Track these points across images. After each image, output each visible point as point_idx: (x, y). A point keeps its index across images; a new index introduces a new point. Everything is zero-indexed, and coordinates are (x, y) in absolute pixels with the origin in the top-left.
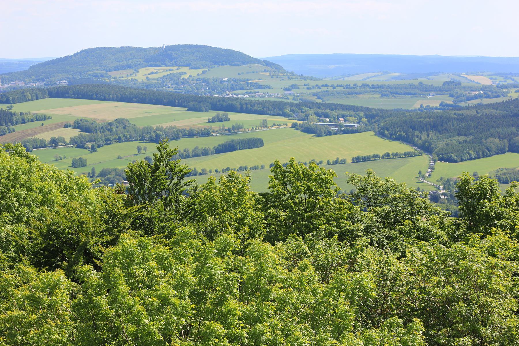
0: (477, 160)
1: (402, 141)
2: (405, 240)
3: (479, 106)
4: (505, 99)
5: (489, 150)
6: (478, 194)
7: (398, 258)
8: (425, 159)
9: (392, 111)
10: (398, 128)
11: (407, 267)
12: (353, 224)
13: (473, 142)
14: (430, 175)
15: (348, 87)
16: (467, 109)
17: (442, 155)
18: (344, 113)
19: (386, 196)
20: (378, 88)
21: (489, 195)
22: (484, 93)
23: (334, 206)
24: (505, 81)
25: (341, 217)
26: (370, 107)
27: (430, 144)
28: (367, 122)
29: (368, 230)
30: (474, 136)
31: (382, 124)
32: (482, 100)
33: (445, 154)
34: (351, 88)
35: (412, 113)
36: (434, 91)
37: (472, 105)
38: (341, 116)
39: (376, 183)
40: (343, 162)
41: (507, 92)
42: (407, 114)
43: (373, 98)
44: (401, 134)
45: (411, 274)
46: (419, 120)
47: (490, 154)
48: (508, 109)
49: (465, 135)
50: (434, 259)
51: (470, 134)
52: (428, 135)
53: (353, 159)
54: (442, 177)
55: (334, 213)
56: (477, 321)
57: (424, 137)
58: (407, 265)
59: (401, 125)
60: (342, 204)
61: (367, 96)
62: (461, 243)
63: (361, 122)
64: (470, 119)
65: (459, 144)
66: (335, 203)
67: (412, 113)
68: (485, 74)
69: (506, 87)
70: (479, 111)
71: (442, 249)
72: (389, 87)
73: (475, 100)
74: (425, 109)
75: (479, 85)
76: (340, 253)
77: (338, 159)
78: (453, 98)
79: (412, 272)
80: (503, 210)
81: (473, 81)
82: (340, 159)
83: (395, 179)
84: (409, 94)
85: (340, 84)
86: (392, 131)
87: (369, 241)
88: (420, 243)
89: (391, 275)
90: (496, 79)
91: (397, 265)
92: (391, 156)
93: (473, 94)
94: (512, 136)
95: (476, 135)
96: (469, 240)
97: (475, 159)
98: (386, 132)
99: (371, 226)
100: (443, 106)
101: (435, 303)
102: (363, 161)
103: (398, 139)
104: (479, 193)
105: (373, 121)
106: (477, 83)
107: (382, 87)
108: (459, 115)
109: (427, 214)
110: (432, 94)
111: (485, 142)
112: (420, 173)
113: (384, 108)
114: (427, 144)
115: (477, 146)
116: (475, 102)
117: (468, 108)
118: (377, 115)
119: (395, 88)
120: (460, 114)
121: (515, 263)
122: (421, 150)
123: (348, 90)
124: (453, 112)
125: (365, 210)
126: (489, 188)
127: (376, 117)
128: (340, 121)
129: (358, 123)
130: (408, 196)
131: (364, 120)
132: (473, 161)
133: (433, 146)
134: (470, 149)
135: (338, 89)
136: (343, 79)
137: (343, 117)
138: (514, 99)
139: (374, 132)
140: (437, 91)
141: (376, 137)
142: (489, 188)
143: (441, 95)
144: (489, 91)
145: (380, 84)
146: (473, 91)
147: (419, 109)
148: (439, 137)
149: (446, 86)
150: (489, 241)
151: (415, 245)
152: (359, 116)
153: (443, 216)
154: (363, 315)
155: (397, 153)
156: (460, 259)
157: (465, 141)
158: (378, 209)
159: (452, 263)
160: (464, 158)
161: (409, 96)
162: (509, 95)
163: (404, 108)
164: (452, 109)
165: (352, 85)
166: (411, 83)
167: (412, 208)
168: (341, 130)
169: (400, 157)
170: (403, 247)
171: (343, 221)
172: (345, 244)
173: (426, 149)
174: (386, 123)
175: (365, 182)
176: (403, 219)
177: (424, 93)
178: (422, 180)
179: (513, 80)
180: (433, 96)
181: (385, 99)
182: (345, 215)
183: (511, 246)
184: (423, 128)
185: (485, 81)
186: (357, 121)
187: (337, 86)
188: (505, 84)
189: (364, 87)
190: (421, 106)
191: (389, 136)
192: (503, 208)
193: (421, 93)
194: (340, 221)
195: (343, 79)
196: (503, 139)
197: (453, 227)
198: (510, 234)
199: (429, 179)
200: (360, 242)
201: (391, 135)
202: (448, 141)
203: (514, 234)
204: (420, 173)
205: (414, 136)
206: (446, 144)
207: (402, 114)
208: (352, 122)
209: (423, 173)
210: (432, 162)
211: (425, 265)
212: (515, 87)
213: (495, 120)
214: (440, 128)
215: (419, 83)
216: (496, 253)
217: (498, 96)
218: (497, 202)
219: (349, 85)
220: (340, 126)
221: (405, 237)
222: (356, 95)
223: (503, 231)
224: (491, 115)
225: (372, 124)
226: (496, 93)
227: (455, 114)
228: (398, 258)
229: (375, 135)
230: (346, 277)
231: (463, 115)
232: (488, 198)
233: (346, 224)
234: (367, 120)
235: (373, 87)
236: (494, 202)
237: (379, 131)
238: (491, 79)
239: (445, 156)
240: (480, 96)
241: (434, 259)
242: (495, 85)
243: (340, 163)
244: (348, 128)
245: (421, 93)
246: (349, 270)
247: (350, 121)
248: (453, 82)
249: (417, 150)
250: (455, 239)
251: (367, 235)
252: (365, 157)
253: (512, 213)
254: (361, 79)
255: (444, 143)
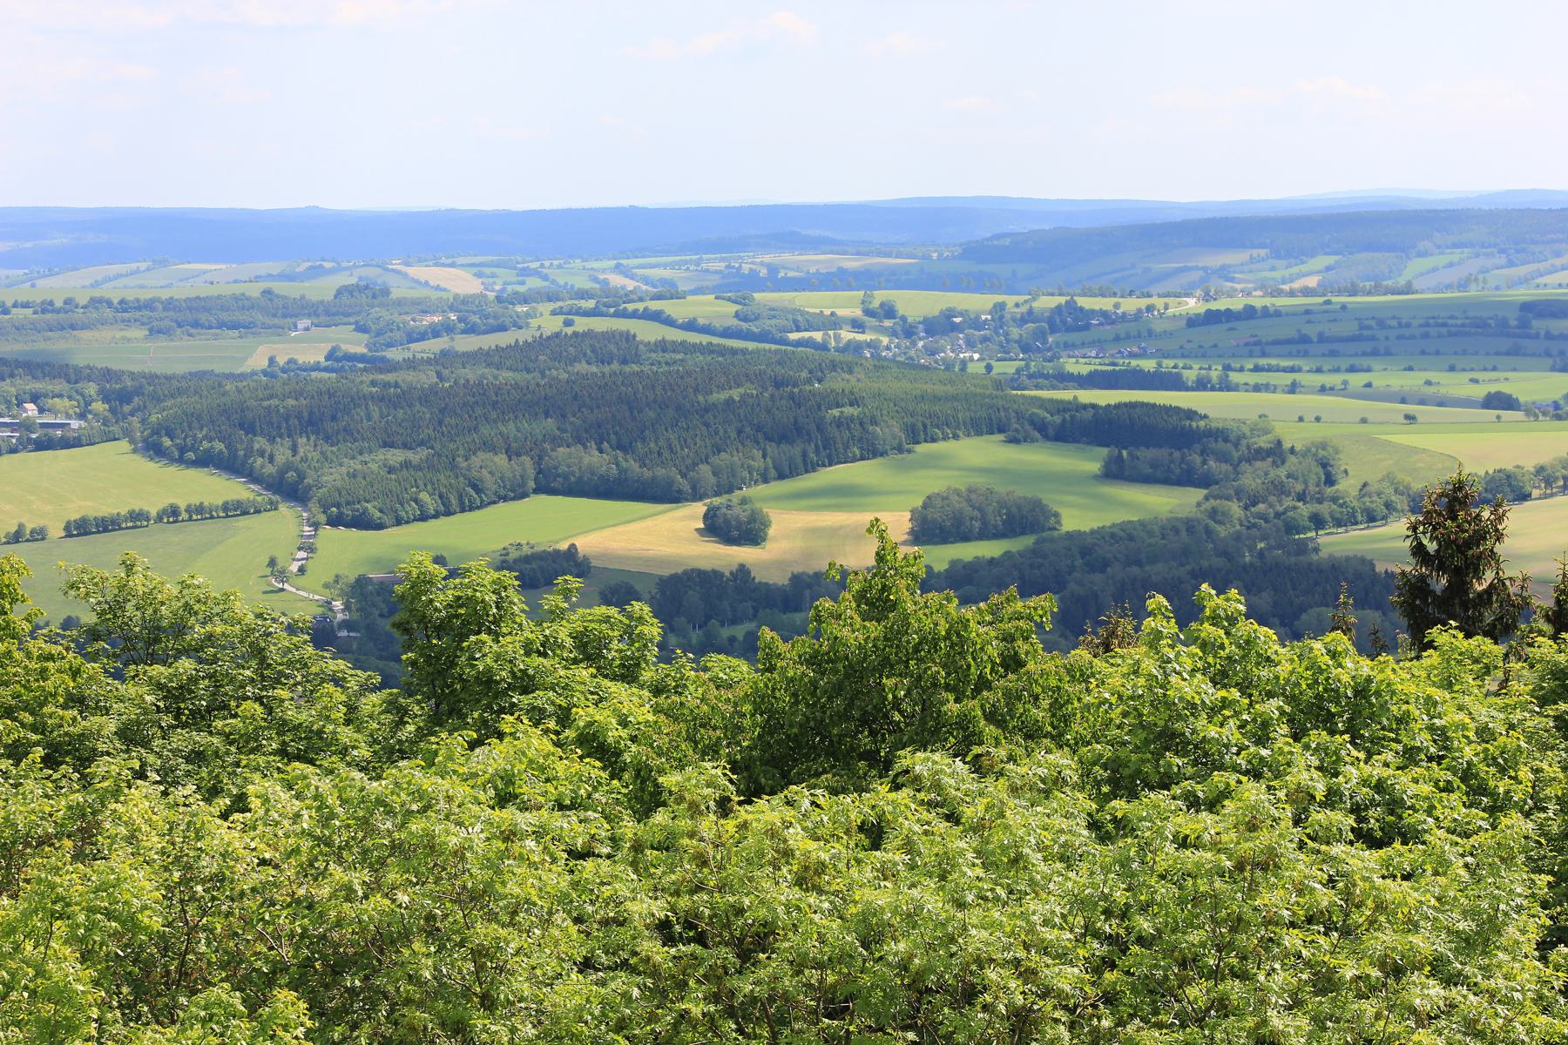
0: (443, 521)
1: (217, 467)
2: (244, 763)
3: (445, 357)
4: (523, 336)
5: (478, 490)
6: (457, 616)
7: (224, 816)
8: (286, 522)
9: (183, 377)
10: (201, 429)
11: (252, 839)
12: (84, 719)
13: (431, 467)
14: (302, 570)
15: (47, 307)
16: (409, 368)
17: (338, 506)
18: (38, 386)
19: (179, 629)
20: (139, 309)
21: (491, 619)
22: (460, 320)
23: (26, 666)
24: (523, 283)
25: (46, 698)
26: (115, 367)
27: (301, 476)
28: (106, 413)
29: (130, 736)
30: (432, 448)
31: (153, 418)
32: (453, 339)
33: (348, 503)
34: (58, 311)
35: (244, 383)
36: (309, 316)
37: (425, 356)
38: (27, 397)
39: (151, 594)
40: (39, 535)
41: (528, 315)
42: (228, 388)
43: (123, 338)
44: (212, 447)
45: (263, 862)
46: (265, 404)
47: (482, 501)
48: (531, 365)
49: (406, 446)
50: (333, 816)
51: (422, 443)
52: (294, 450)
53: (67, 528)
54: (340, 573)
55: (24, 686)
56: (467, 993)
57: (282, 454)
58: (252, 834)
59: (213, 422)
60: (50, 657)
61: (106, 334)
62: (414, 762)
63: (90, 412)
64: (420, 398)
65: (389, 473)
66: (29, 656)
67: (244, 383)
68: (460, 261)
69: (525, 300)
70: (446, 373)
71: (358, 784)
72: (169, 304)
73: (433, 341)
74: (284, 370)
75: (444, 295)
76: (52, 806)
77: (21, 526)
78: (367, 336)
79: (267, 856)
80: (535, 665)
81: (426, 284)
82: (29, 527)
83: (207, 580)
84: (234, 326)
85: (22, 299)
86: (185, 439)
87: (136, 765)
88: (289, 769)
89: (208, 866)
90: (494, 276)
91: (223, 835)
92: (185, 516)
93: (428, 320)
94: (547, 446)
95: (438, 446)
96: (436, 753)
97: (436, 516)
98: (167, 442)
99: (138, 723)
100: (338, 360)
101: (339, 945)
102: (99, 532)
103: (205, 461)
104: (461, 615)
105: (127, 408)
106: (438, 288)
107: (149, 305)
108: (387, 385)
109: (307, 681)
110: (303, 323)
111: (464, 465)
112: (272, 563)
113: (159, 369)
114: (291, 475)
115: (442, 477)
116: (434, 346)
117: (412, 364)
118: (138, 392)
119: (190, 309)
120: (389, 383)
121: (575, 818)
122: (274, 493)
123: (49, 316)
124: (368, 378)
125: (118, 675)
126: (490, 598)
127: (136, 399)
128: (26, 410)
129: (82, 416)
130: (250, 630)
131: (99, 406)
132: (432, 523)
133: (308, 481)
134: (422, 487)
135: (19, 313)
136: (33, 286)
137: (35, 399)
138: (549, 334)
139: (130, 442)
140: (317, 315)
141: (137, 457)
142: (490, 598)
143: (330, 326)
144: (474, 313)
145: (145, 295)
146: (425, 312)
147: (265, 373)
148: (329, 454)
149: (345, 299)
150: (494, 757)
151: (276, 775)
152: (82, 395)
153: (356, 688)
154: (125, 990)
155: (202, 503)
156: (410, 813)
157: (406, 465)
158: (157, 670)
159: (389, 825)
160: (403, 514)
161: (236, 333)
162: (534, 323)
163: (219, 368)
164: (365, 370)
165: (59, 304)
166: (238, 293)
167: (263, 662)
168: (29, 439)
169: (212, 517)
170: (239, 781)
171: (53, 709)
172: (64, 776)
173: (290, 489)
174: (165, 414)
175: (116, 592)
176: (237, 699)
177: (276, 321)
178: (281, 586)
179: (545, 278)
180: (307, 329)
181: (162, 342)
182: (60, 690)
183: (561, 768)
184: (279, 427)
185: (460, 282)
186: (77, 410)
187: (15, 305)
188: (521, 289)
189: (96, 308)
190: (272, 361)
191: (176, 455)
192: (534, 655)
193: (269, 321)
194: (45, 710)
195: (33, 286)
196: (518, 455)
197: (388, 718)
198: (557, 733)
199: (301, 581)
200: (108, 767)
201: (182, 450)
202: (356, 465)
203: (570, 734)
204: (272, 563)
205: (252, 452)
206: (348, 473)
207: (213, 388)
208: (63, 414)
209: (280, 564)
210: (307, 528)
211: (309, 835)
212: (550, 298)
213: (494, 398)
214: (330, 426)
215: (264, 292)
216: (518, 791)
217: (502, 328)
218: (518, 638)
219: (51, 303)
220: (27, 426)
221: (241, 753)
222: (74, 333)
223: (536, 725)
224: (481, 383)
225: (124, 417)
226: (496, 317)
227: (373, 383)
228: (224, 816)
229: (135, 451)
230: (72, 880)
231: (396, 385)
232: (489, 628)
233: (62, 719)
234: (107, 406)
235: (124, 306)
236: (509, 639)
237: (145, 440)
238: (478, 275)
239: (347, 512)
240: (448, 329)
241: (333, 816)
242: (492, 296)
243: (28, 541)
244: (50, 431)
245: (269, 321)
246: (78, 856)
247: (55, 412)
248: (367, 287)
249: (261, 495)
250: (392, 753)
251: (128, 751)
252: (103, 519)
253: (562, 673)
254: (87, 283)
255: (344, 470)
